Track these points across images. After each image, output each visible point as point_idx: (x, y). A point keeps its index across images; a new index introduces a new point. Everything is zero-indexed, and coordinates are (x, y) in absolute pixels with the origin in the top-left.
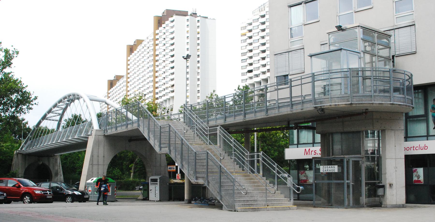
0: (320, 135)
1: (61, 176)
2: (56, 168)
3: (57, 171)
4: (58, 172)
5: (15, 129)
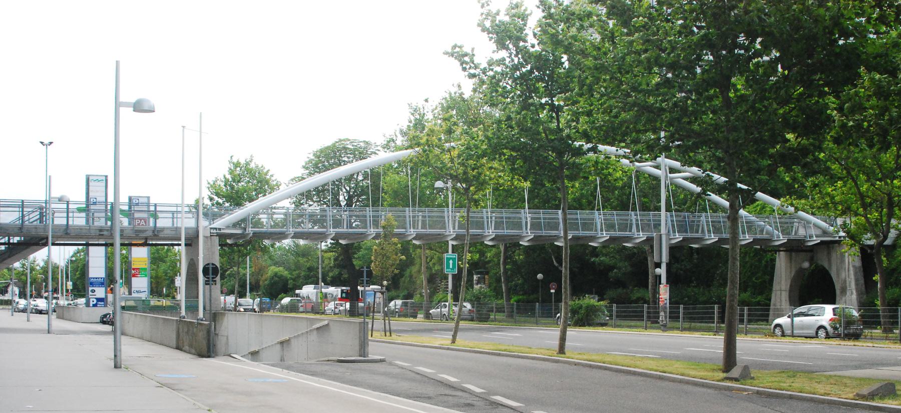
0: (759, 193)
1: (852, 293)
2: (843, 275)
3: (845, 281)
4: (846, 284)
5: (684, 96)
